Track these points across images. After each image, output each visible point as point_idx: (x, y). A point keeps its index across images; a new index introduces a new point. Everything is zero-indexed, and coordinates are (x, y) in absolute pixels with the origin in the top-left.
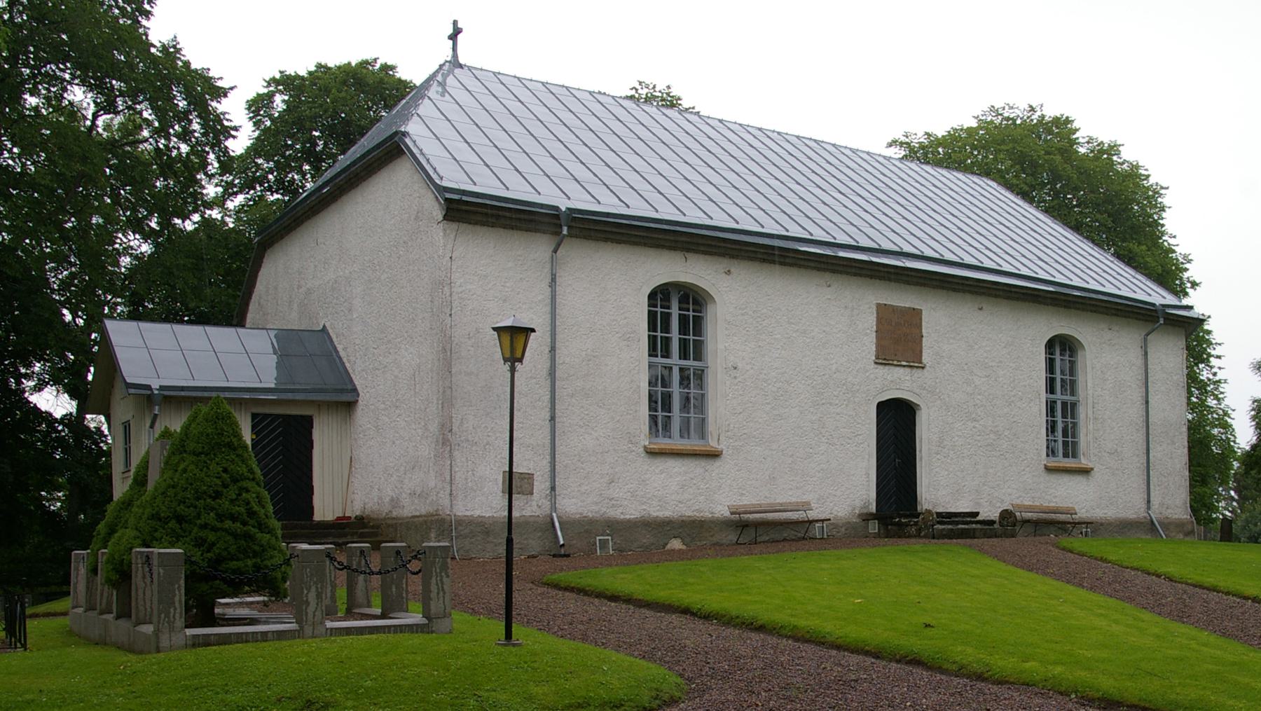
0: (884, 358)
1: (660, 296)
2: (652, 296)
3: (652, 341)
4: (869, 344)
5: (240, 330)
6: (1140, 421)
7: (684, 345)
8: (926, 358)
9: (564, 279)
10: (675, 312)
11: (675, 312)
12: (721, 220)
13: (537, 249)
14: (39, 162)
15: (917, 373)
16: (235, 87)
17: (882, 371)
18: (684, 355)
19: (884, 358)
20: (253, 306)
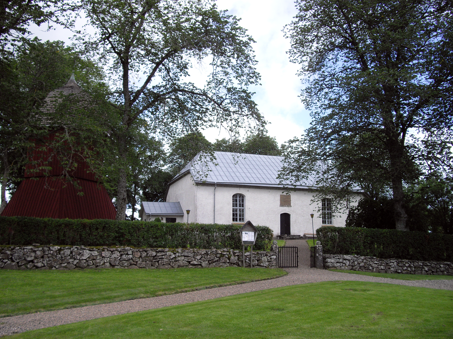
0: (282, 205)
1: (235, 196)
2: (233, 196)
3: (233, 204)
4: (279, 203)
5: (165, 203)
6: (213, 210)
7: (240, 204)
8: (292, 205)
9: (216, 193)
10: (238, 199)
11: (238, 199)
12: (263, 182)
13: (212, 189)
14: (131, 94)
15: (290, 208)
16: (255, 93)
17: (281, 208)
18: (240, 206)
19: (282, 205)
20: (168, 196)
